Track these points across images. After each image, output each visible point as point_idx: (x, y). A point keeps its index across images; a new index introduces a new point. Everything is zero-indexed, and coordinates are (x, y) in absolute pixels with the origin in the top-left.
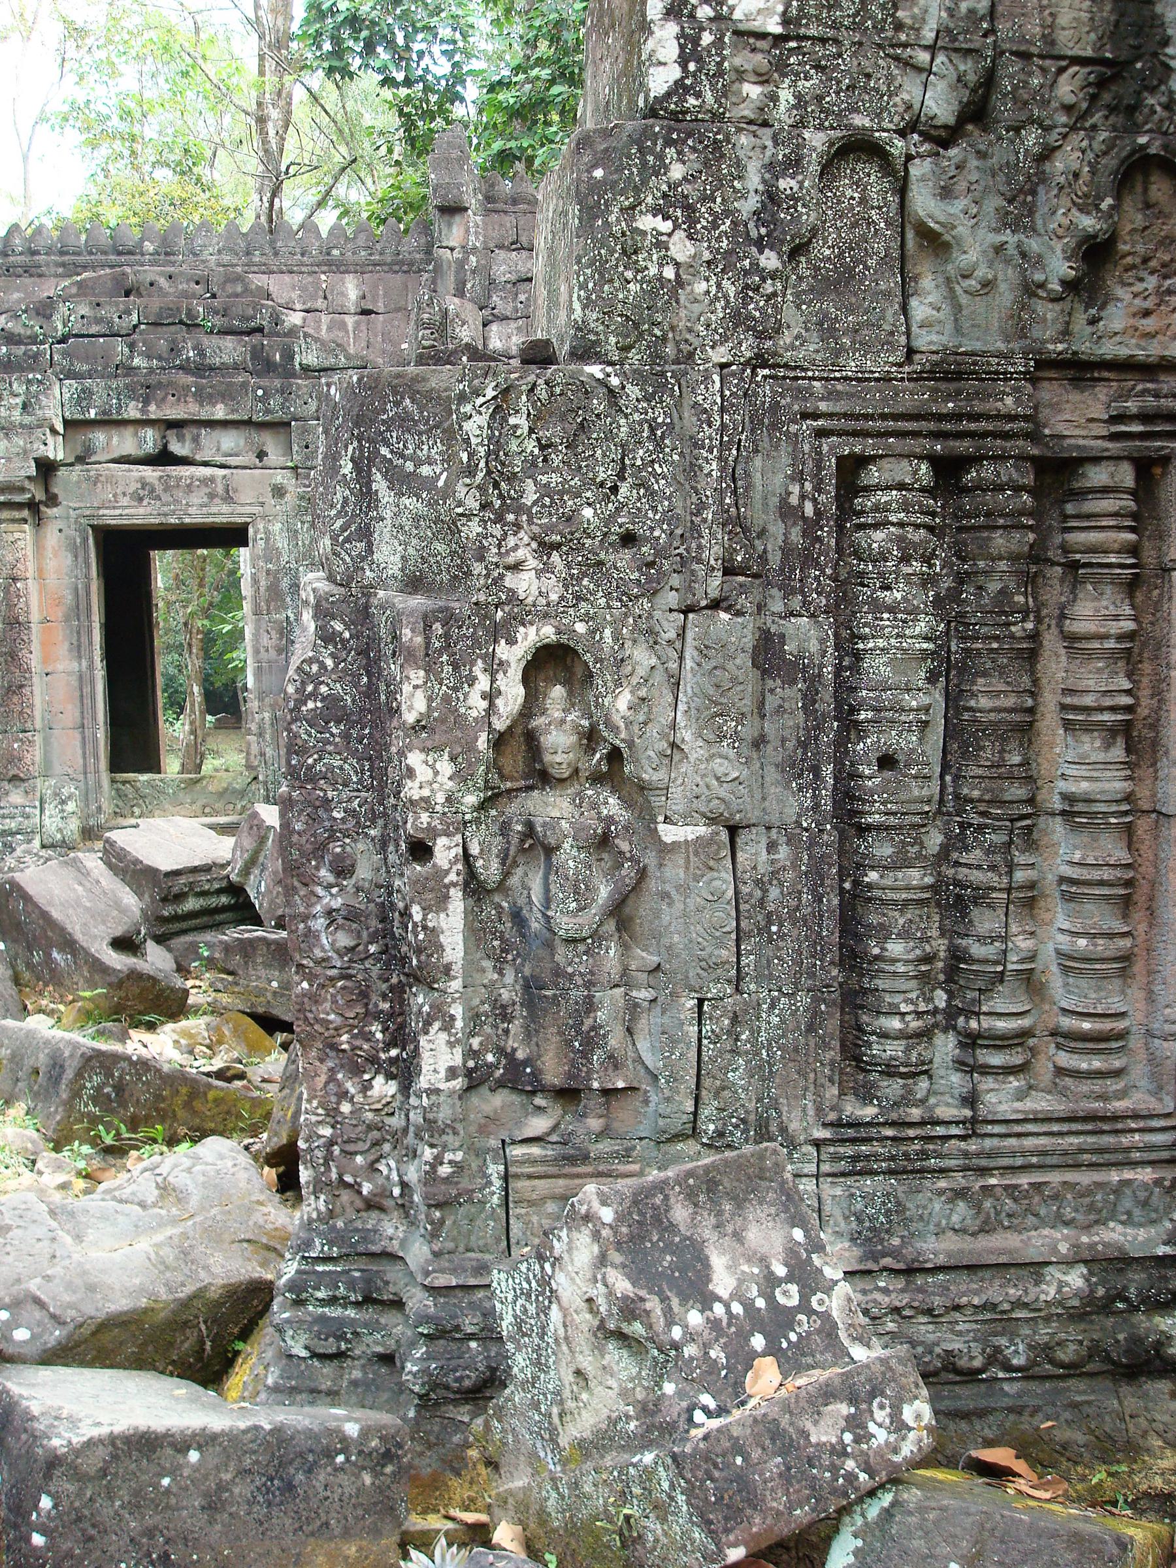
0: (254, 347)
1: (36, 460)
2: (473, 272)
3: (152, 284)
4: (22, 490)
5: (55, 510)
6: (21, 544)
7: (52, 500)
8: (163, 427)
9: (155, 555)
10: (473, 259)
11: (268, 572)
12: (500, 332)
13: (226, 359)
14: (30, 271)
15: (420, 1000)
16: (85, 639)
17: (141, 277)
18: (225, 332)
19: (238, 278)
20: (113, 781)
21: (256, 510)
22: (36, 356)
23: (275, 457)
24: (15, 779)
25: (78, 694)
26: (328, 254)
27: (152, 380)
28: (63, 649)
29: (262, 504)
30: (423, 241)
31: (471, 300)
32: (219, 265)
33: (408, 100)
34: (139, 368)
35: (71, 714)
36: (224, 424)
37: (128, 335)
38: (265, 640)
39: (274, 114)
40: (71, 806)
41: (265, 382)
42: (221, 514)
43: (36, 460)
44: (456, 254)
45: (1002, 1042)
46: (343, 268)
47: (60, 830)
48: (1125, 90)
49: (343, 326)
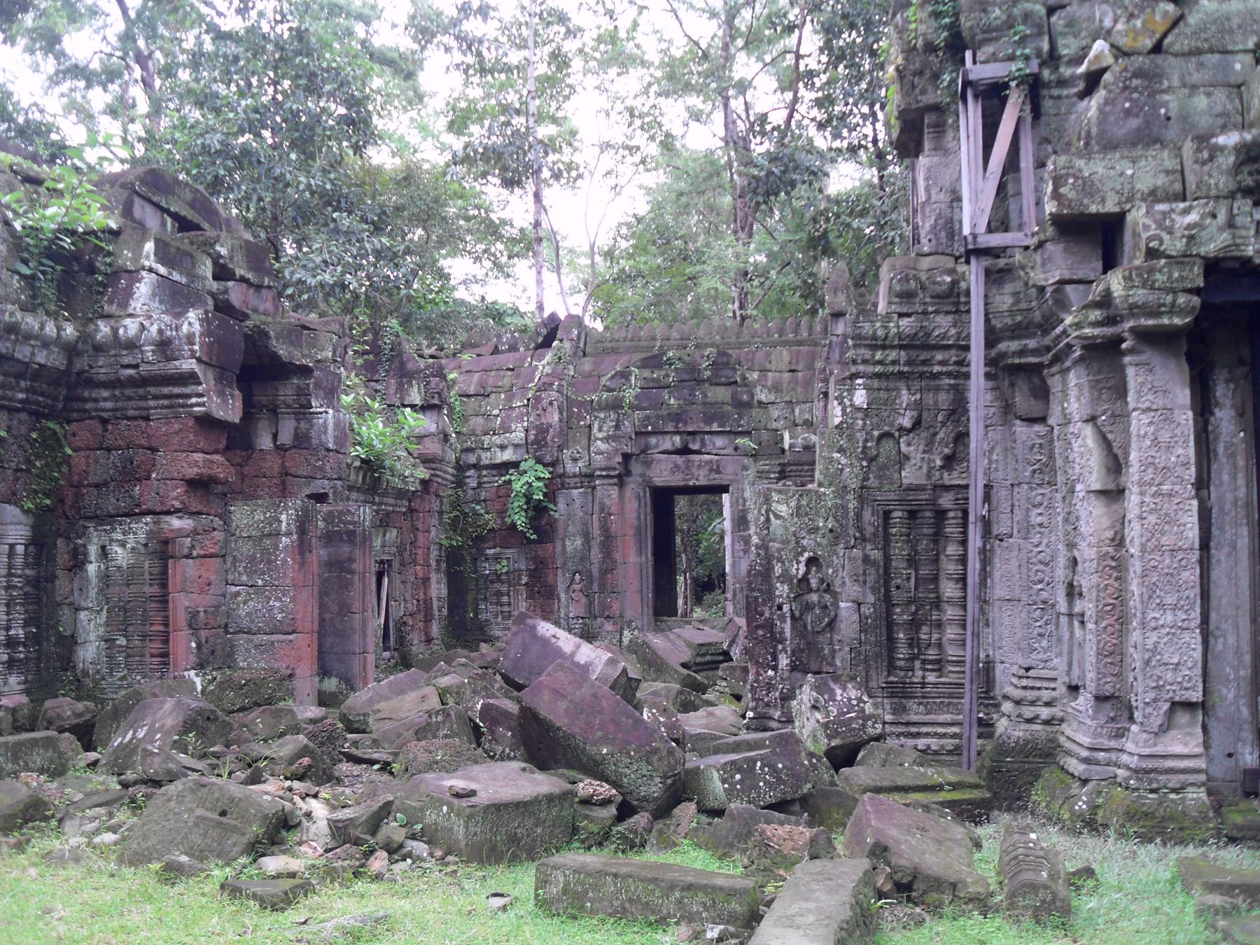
4: (615, 469)
9: (677, 497)
15: (780, 647)
42: (717, 480)
45: (931, 662)
48: (956, 416)
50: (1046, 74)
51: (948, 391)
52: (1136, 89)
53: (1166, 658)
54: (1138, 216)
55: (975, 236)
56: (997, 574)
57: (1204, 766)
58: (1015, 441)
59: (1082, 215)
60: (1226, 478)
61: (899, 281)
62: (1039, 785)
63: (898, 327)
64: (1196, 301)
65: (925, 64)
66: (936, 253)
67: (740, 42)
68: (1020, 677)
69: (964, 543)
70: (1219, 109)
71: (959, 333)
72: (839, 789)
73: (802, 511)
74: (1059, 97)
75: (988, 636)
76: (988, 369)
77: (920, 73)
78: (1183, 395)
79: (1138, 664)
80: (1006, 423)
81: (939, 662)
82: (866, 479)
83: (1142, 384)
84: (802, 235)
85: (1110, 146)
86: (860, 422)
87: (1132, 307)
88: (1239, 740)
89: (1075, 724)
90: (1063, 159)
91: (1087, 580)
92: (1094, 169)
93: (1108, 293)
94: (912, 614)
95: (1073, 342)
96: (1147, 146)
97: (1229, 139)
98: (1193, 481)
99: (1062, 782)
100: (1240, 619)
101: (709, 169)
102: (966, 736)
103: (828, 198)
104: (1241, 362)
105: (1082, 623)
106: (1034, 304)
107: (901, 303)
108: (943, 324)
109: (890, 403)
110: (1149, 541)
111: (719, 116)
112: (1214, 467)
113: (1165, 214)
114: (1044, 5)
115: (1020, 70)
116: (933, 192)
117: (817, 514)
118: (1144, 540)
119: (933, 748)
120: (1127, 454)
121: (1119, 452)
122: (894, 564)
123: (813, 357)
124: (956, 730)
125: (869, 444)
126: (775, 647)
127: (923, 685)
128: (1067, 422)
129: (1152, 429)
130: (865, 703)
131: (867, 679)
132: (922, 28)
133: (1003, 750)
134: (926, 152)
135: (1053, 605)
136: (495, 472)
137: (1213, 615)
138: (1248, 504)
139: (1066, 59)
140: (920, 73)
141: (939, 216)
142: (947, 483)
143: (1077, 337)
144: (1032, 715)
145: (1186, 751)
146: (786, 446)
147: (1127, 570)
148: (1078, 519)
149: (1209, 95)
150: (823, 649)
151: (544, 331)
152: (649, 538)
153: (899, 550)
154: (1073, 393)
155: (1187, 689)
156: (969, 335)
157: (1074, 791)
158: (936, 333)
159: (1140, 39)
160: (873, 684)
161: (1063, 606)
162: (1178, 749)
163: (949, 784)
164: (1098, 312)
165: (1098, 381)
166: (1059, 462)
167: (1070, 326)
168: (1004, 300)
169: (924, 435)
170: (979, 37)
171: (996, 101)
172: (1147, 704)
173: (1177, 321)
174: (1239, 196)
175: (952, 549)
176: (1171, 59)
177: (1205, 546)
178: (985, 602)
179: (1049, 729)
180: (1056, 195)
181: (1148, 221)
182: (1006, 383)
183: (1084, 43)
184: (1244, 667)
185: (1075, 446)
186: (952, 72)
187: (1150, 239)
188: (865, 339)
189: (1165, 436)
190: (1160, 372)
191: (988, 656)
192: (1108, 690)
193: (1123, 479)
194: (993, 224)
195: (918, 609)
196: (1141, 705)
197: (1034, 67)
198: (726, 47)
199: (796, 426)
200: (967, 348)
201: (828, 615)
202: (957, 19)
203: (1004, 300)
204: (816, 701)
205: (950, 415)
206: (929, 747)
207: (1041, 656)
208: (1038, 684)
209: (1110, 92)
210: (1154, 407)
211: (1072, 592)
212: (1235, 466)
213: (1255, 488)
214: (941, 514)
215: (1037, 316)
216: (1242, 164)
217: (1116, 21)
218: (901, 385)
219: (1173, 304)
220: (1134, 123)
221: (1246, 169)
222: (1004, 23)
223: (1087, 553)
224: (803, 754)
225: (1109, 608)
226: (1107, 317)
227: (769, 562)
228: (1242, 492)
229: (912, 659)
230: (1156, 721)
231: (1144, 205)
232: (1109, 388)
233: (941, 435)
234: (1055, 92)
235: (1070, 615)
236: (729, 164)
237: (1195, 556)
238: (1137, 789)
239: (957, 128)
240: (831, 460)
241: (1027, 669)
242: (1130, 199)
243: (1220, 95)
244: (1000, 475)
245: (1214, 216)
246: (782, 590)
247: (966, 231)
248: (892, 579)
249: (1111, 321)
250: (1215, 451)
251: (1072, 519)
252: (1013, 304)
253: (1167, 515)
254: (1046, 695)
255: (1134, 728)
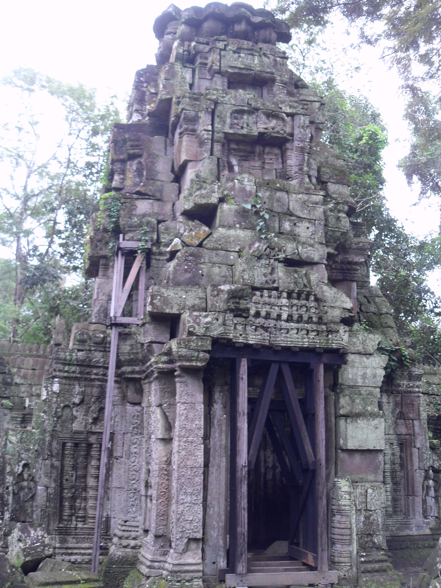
15: (6, 508)
48: (100, 400)
50: (154, 249)
51: (97, 387)
52: (190, 261)
53: (187, 518)
54: (185, 316)
55: (115, 317)
56: (114, 475)
57: (202, 569)
58: (126, 413)
59: (162, 313)
60: (217, 435)
61: (79, 334)
62: (127, 579)
63: (77, 356)
64: (208, 356)
65: (103, 237)
66: (98, 323)
67: (29, 212)
68: (122, 525)
69: (99, 460)
70: (223, 274)
71: (105, 361)
72: (26, 585)
73: (23, 440)
74: (159, 260)
75: (108, 505)
76: (116, 379)
77: (100, 241)
78: (200, 397)
79: (174, 520)
80: (123, 404)
81: (84, 517)
82: (55, 427)
83: (182, 391)
84: (47, 306)
85: (177, 284)
86: (55, 399)
87: (180, 356)
88: (218, 555)
89: (146, 549)
90: (156, 288)
91: (154, 481)
92: (169, 294)
93: (170, 349)
94: (73, 493)
95: (154, 370)
96: (193, 286)
97: (225, 287)
98: (202, 436)
99: (138, 578)
100: (221, 499)
101: (6, 269)
102: (94, 554)
103: (61, 290)
104: (226, 384)
105: (151, 500)
106: (139, 350)
107: (79, 345)
108: (97, 356)
109: (70, 391)
110: (181, 463)
111: (15, 244)
112: (212, 430)
113: (197, 316)
114: (156, 219)
115: (143, 246)
116: (100, 295)
117: (30, 442)
118: (179, 462)
119: (79, 560)
120: (174, 422)
121: (171, 421)
122: (66, 468)
123: (44, 364)
124: (90, 551)
125: (58, 410)
126: (3, 508)
127: (76, 528)
128: (150, 406)
129: (185, 412)
130: (46, 538)
131: (49, 525)
132: (103, 221)
133: (112, 562)
134: (100, 276)
135: (139, 491)
137: (209, 497)
138: (226, 447)
139: (164, 244)
140: (100, 241)
141: (101, 306)
142: (94, 431)
143: (156, 368)
144: (126, 544)
145: (194, 562)
146: (27, 405)
147: (172, 476)
148: (151, 451)
149: (220, 267)
150: (27, 510)
153: (68, 462)
154: (153, 393)
155: (195, 532)
156: (108, 363)
157: (143, 582)
158: (94, 360)
159: (194, 240)
160: (51, 528)
161: (143, 492)
162: (191, 561)
163: (83, 580)
164: (165, 357)
165: (164, 388)
166: (145, 424)
167: (153, 362)
168: (126, 348)
169: (85, 407)
170: (127, 229)
171: (132, 258)
172: (177, 539)
173: (199, 364)
174: (228, 312)
175: (94, 462)
176: (205, 250)
177: (206, 465)
178: (108, 488)
179: (134, 551)
180: (152, 303)
181: (189, 319)
182: (125, 385)
183: (171, 238)
184: (222, 522)
185: (152, 417)
186: (114, 242)
187: (190, 327)
188: (61, 360)
189: (191, 415)
190: (190, 386)
191: (108, 515)
192: (161, 532)
193: (172, 434)
194: (125, 312)
195: (76, 491)
196: (175, 540)
197: (149, 245)
198: (22, 214)
199: (33, 396)
200: (107, 368)
201: (32, 493)
202: (119, 220)
203: (126, 348)
204: (21, 537)
205: (97, 399)
206: (76, 560)
207: (132, 515)
208: (130, 529)
209: (179, 260)
210: (187, 402)
211: (147, 486)
212: (221, 430)
213: (229, 440)
214: (90, 446)
215: (140, 356)
216: (230, 299)
217: (185, 231)
218: (76, 383)
219: (198, 357)
220: (188, 275)
221: (232, 301)
222: (138, 224)
223: (154, 467)
224: (8, 566)
225: (163, 493)
226: (170, 360)
227: (4, 465)
228: (224, 442)
229: (71, 516)
230: (181, 548)
231: (188, 311)
232: (168, 392)
233: (93, 408)
234: (158, 257)
235: (146, 496)
236: (16, 269)
237: (201, 471)
238: (171, 581)
239: (113, 267)
240: (39, 417)
241: (126, 522)
242: (183, 308)
243: (224, 268)
244: (119, 428)
245: (217, 320)
246: (9, 479)
247: (112, 315)
248: (64, 476)
249: (171, 362)
250: (213, 423)
251: (149, 451)
252: (130, 350)
253: (190, 451)
254: (133, 534)
255: (172, 551)
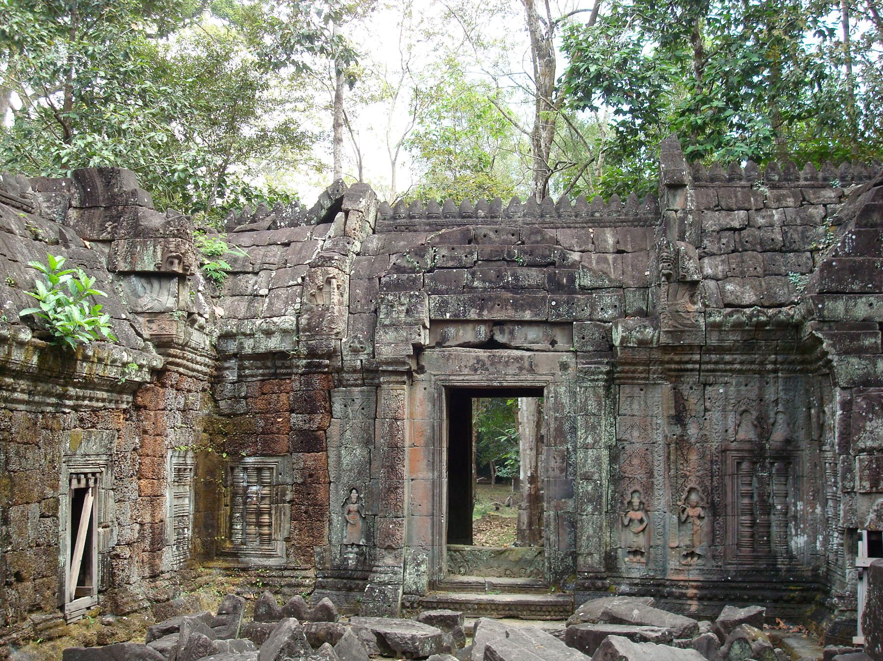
0: (550, 275)
1: (413, 345)
2: (691, 225)
3: (485, 236)
5: (422, 375)
6: (401, 397)
7: (421, 370)
8: (491, 324)
10: (690, 217)
11: (556, 418)
12: (710, 263)
13: (532, 282)
14: (409, 228)
16: (437, 458)
17: (478, 232)
18: (530, 265)
19: (539, 232)
20: (449, 550)
21: (549, 378)
22: (414, 281)
23: (561, 344)
24: (389, 548)
25: (430, 493)
26: (592, 216)
27: (486, 295)
28: (423, 464)
29: (553, 375)
30: (653, 206)
31: (690, 243)
32: (524, 224)
33: (623, 123)
34: (477, 288)
35: (426, 506)
36: (530, 323)
37: (471, 267)
38: (552, 463)
39: (544, 134)
40: (423, 568)
41: (556, 297)
42: (527, 380)
43: (413, 345)
44: (679, 214)
46: (602, 224)
47: (415, 583)
49: (606, 260)
136: (259, 364)
151: (328, 204)
152: (445, 449)
